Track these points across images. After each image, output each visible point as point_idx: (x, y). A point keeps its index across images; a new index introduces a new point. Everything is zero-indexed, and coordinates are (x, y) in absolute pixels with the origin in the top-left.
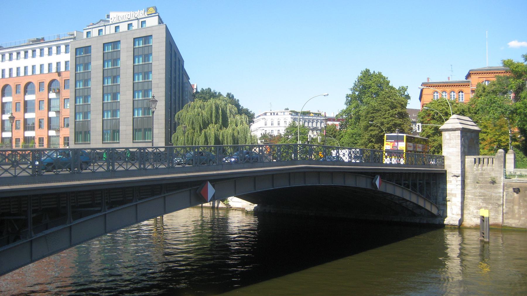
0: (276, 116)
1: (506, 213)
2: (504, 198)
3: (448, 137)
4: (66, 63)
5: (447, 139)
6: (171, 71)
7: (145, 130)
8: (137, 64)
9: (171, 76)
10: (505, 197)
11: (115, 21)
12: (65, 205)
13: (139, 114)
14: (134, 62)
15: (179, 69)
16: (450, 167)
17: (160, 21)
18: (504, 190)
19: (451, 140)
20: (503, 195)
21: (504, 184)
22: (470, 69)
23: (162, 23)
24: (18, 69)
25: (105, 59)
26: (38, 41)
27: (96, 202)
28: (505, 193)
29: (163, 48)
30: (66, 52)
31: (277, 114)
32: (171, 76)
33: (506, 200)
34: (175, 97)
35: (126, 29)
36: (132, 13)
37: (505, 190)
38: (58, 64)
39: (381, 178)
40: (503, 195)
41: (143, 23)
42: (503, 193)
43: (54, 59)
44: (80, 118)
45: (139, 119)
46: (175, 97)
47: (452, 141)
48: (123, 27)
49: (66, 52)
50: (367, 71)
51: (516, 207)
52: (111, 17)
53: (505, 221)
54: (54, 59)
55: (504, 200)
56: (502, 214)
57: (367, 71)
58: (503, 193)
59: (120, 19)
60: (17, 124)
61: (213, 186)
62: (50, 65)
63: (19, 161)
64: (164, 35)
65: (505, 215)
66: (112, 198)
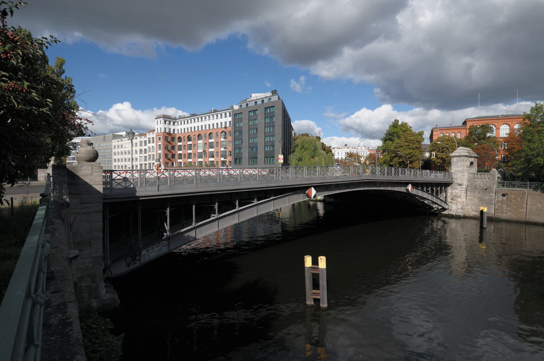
0: (340, 149)
1: (497, 209)
2: (496, 200)
3: (455, 161)
4: (230, 122)
5: (455, 162)
6: (285, 125)
7: (255, 158)
8: (266, 122)
9: (285, 128)
10: (496, 199)
11: (255, 99)
12: (214, 201)
13: (268, 149)
14: (265, 121)
15: (289, 124)
16: (456, 179)
17: (279, 98)
18: (495, 195)
19: (458, 162)
20: (495, 198)
21: (496, 191)
22: (466, 119)
23: (280, 99)
24: (198, 127)
25: (250, 119)
26: (215, 111)
27: (251, 197)
28: (496, 197)
29: (281, 113)
30: (230, 116)
31: (341, 148)
32: (285, 128)
33: (497, 201)
34: (287, 140)
35: (261, 103)
36: (263, 94)
37: (496, 195)
38: (226, 122)
39: (412, 185)
40: (495, 198)
41: (270, 99)
42: (495, 196)
43: (223, 120)
44: (237, 151)
45: (268, 152)
46: (287, 140)
47: (458, 163)
48: (259, 102)
49: (230, 116)
50: (397, 121)
51: (505, 206)
52: (252, 97)
53: (496, 214)
54: (223, 120)
55: (496, 201)
56: (494, 210)
57: (397, 121)
58: (495, 196)
59: (257, 98)
60: (457, 155)
61: (315, 189)
62: (221, 123)
63: (233, 174)
64: (281, 106)
65: (496, 210)
66: (242, 197)
